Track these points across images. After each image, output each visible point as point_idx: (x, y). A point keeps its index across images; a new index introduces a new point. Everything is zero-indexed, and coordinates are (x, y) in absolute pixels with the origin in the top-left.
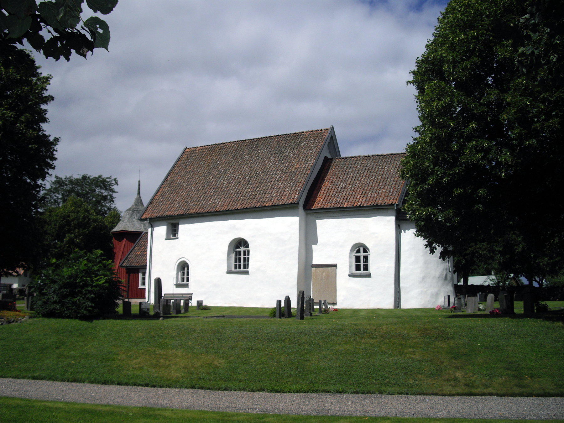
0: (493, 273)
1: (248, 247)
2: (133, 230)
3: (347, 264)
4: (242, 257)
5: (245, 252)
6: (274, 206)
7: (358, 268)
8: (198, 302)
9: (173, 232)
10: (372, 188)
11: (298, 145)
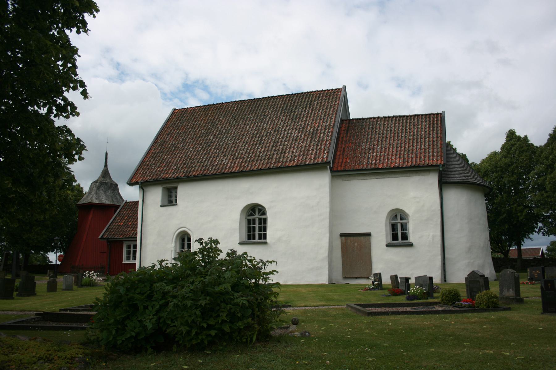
0: (228, 258)
1: (264, 213)
2: (101, 202)
3: (384, 233)
4: (257, 226)
5: (260, 220)
6: (300, 166)
7: (395, 237)
8: (391, 277)
9: (170, 200)
10: (407, 149)
11: (310, 104)
